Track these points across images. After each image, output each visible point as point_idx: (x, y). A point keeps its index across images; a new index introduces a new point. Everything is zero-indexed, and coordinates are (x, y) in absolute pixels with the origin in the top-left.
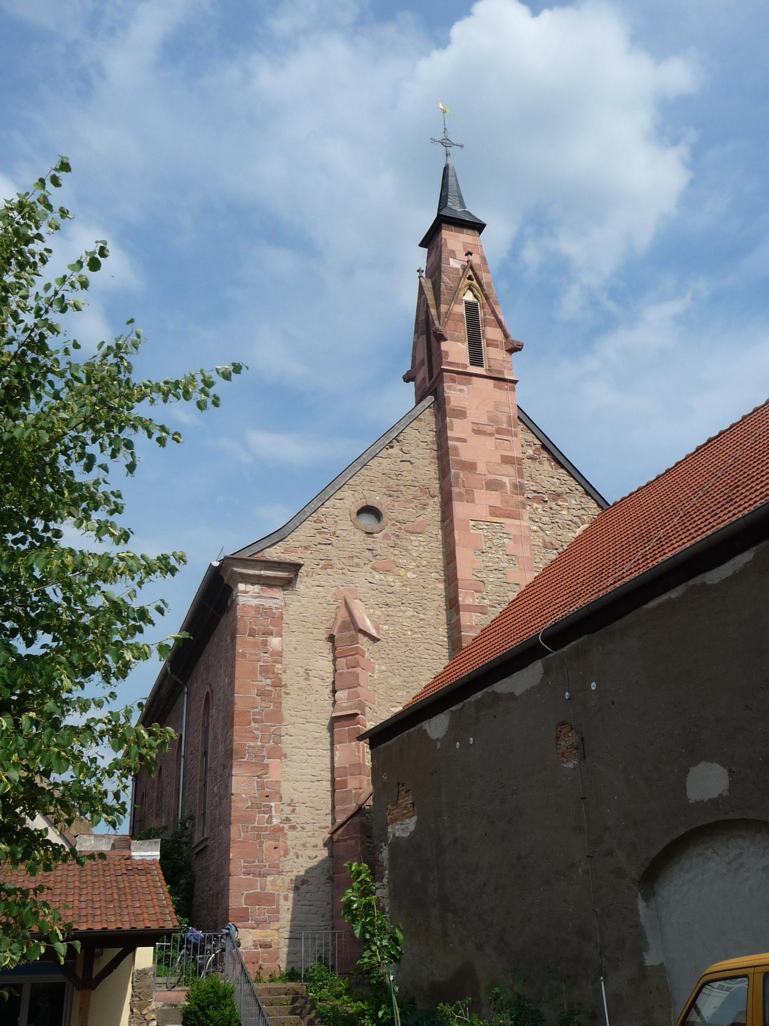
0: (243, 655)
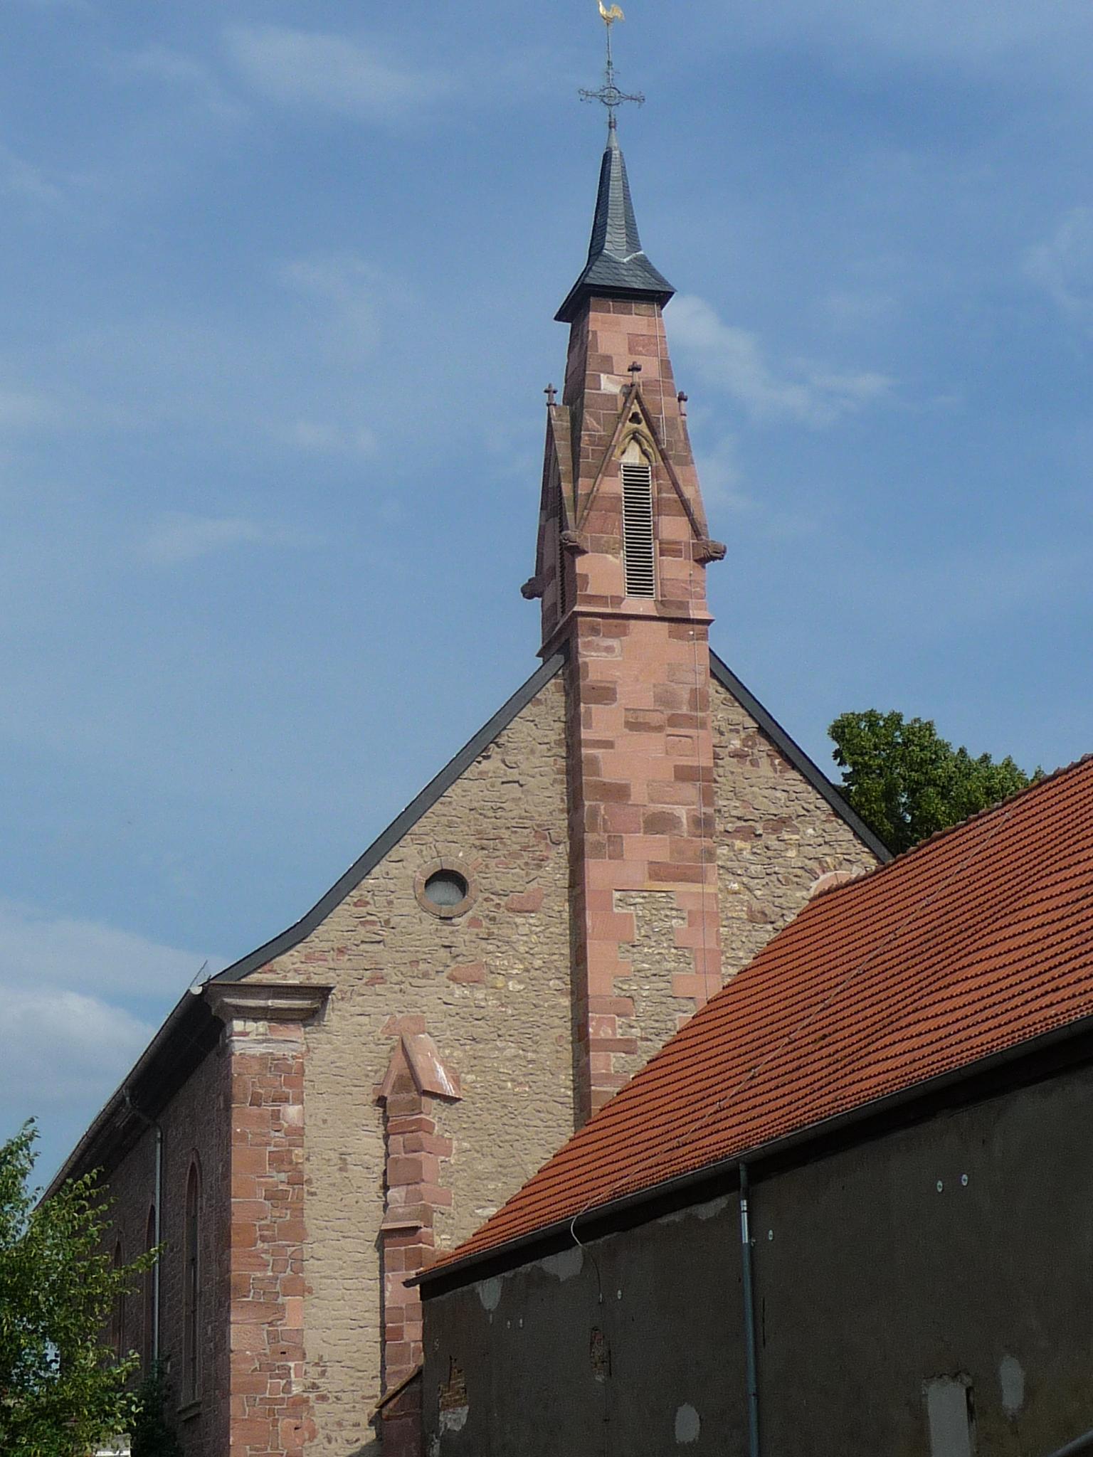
0: (243, 1137)
